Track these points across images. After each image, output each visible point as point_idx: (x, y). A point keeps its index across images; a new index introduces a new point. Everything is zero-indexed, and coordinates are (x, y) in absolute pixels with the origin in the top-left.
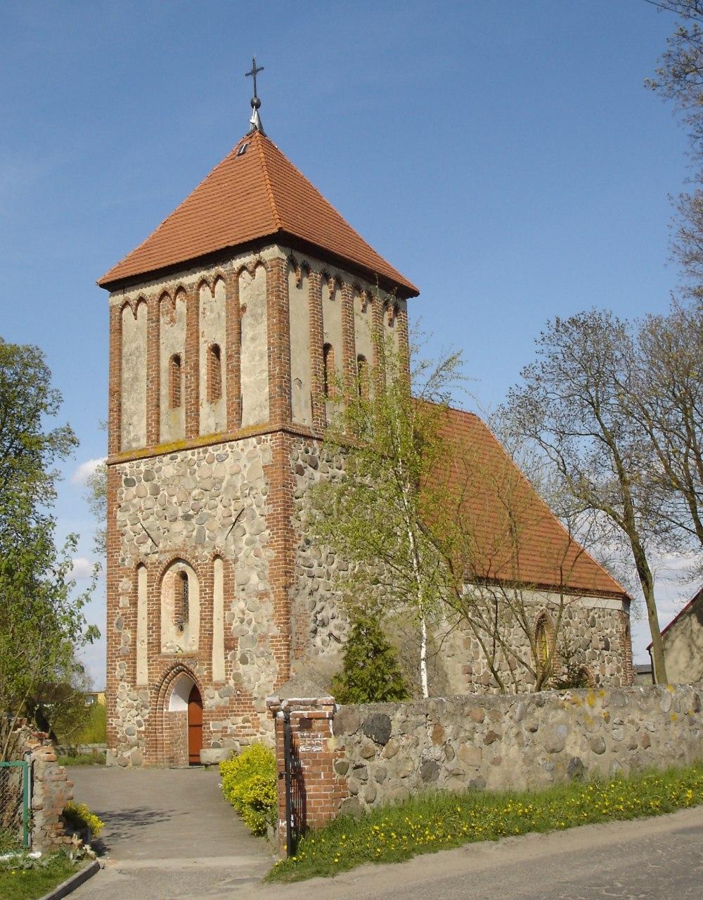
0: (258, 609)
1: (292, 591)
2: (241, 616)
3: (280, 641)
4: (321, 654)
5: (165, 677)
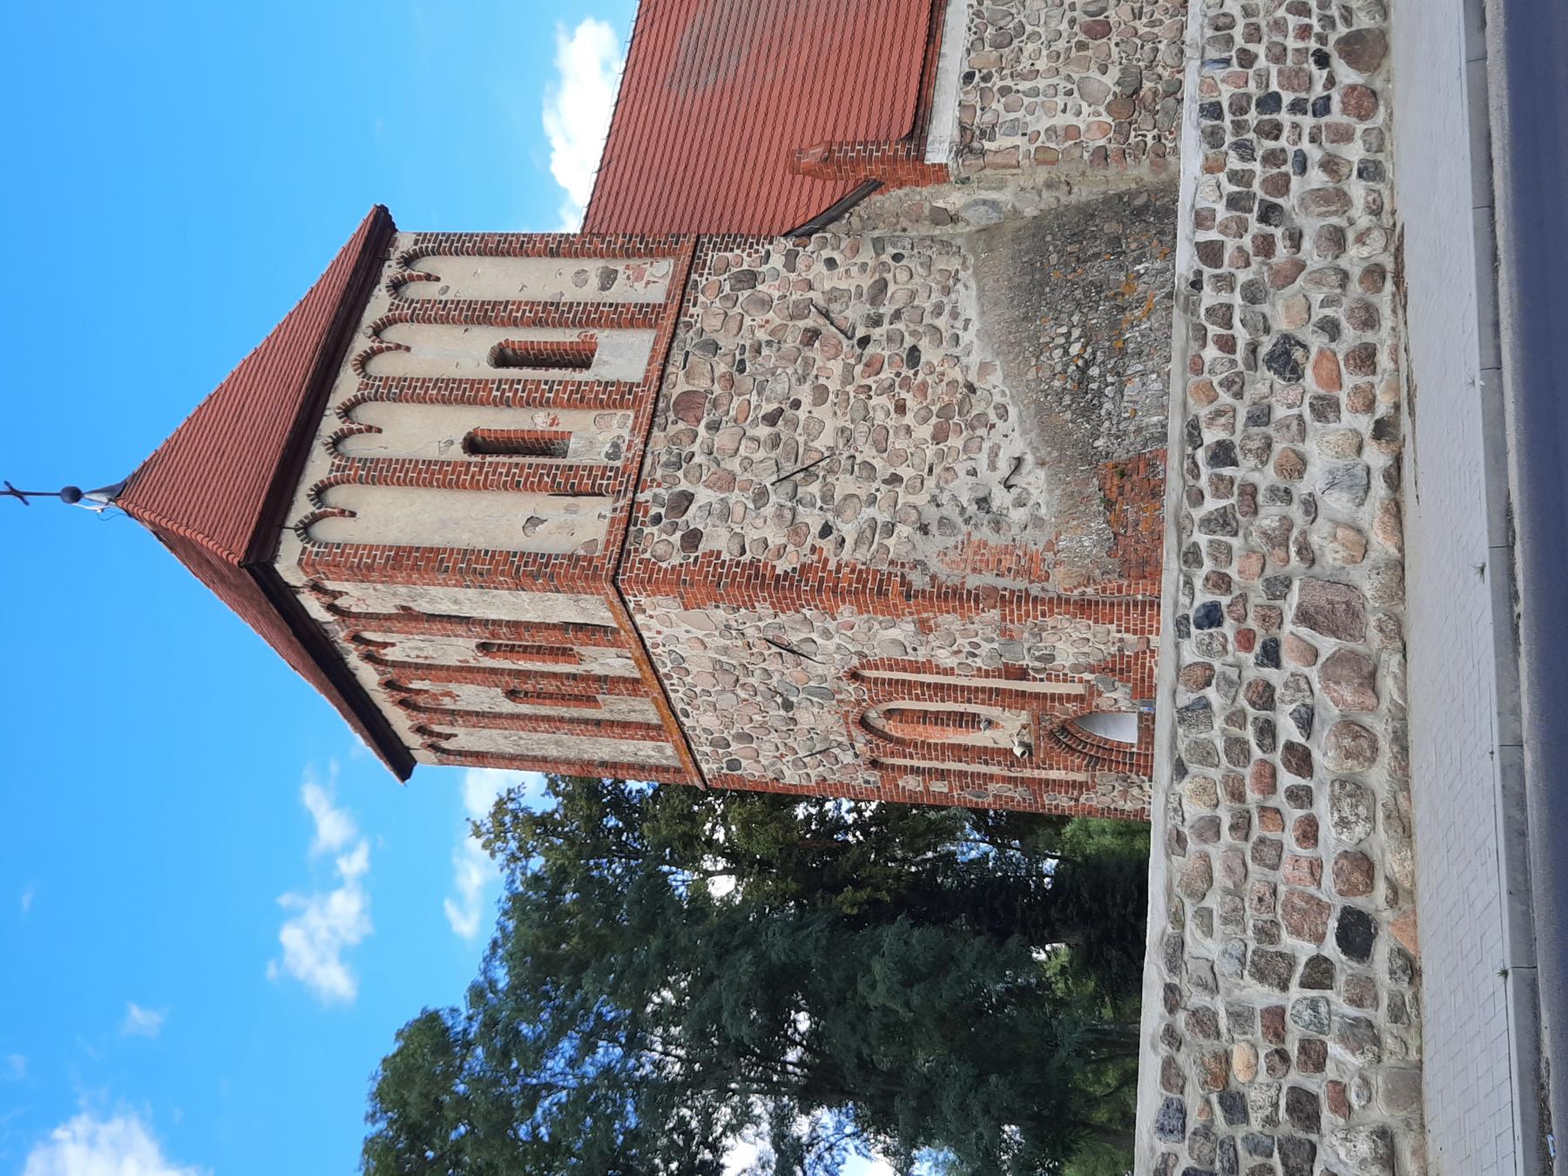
0: (949, 633)
1: (918, 580)
2: (963, 655)
3: (1012, 611)
4: (1043, 511)
5: (1075, 750)
